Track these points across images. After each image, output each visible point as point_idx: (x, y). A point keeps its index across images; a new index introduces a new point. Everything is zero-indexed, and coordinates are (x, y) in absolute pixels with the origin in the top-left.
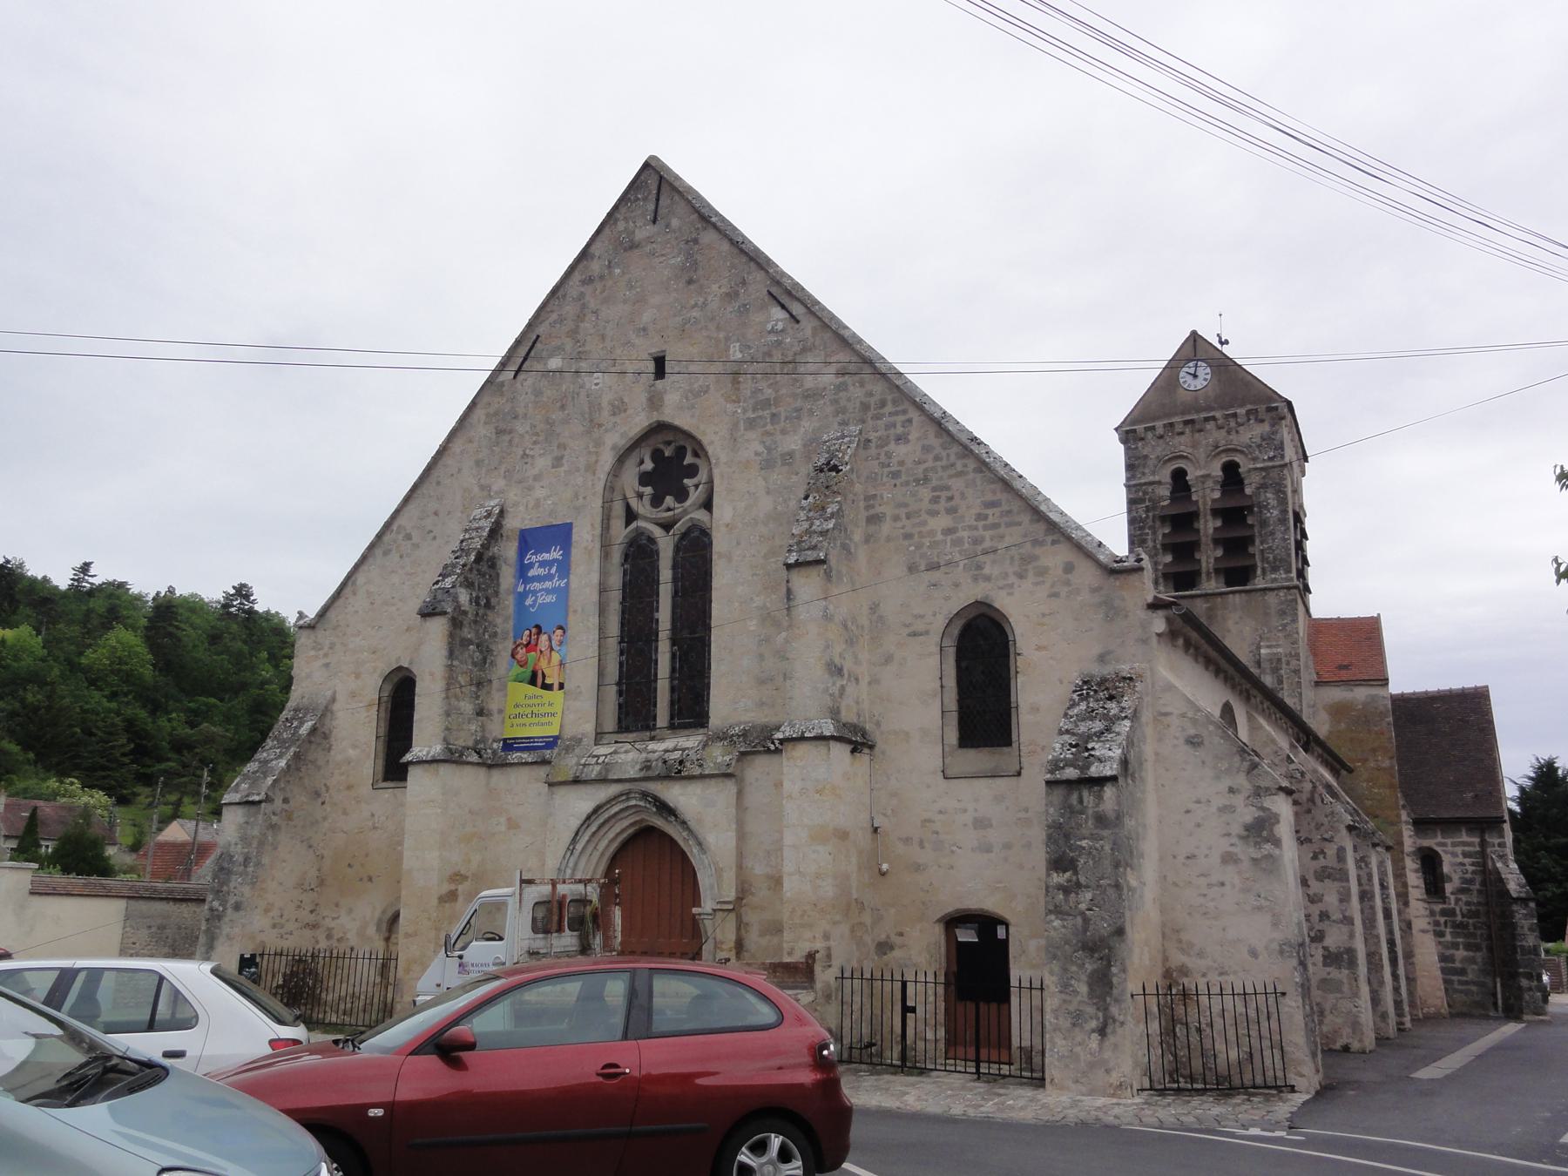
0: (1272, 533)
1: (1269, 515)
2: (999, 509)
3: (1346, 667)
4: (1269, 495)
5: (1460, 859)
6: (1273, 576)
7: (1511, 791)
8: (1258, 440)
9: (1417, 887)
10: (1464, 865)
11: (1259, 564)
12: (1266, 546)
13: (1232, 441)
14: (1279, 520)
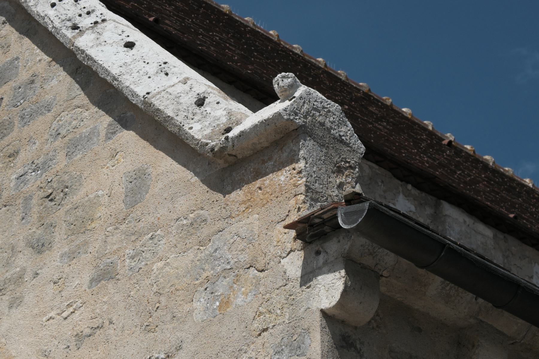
2: (12, 84)
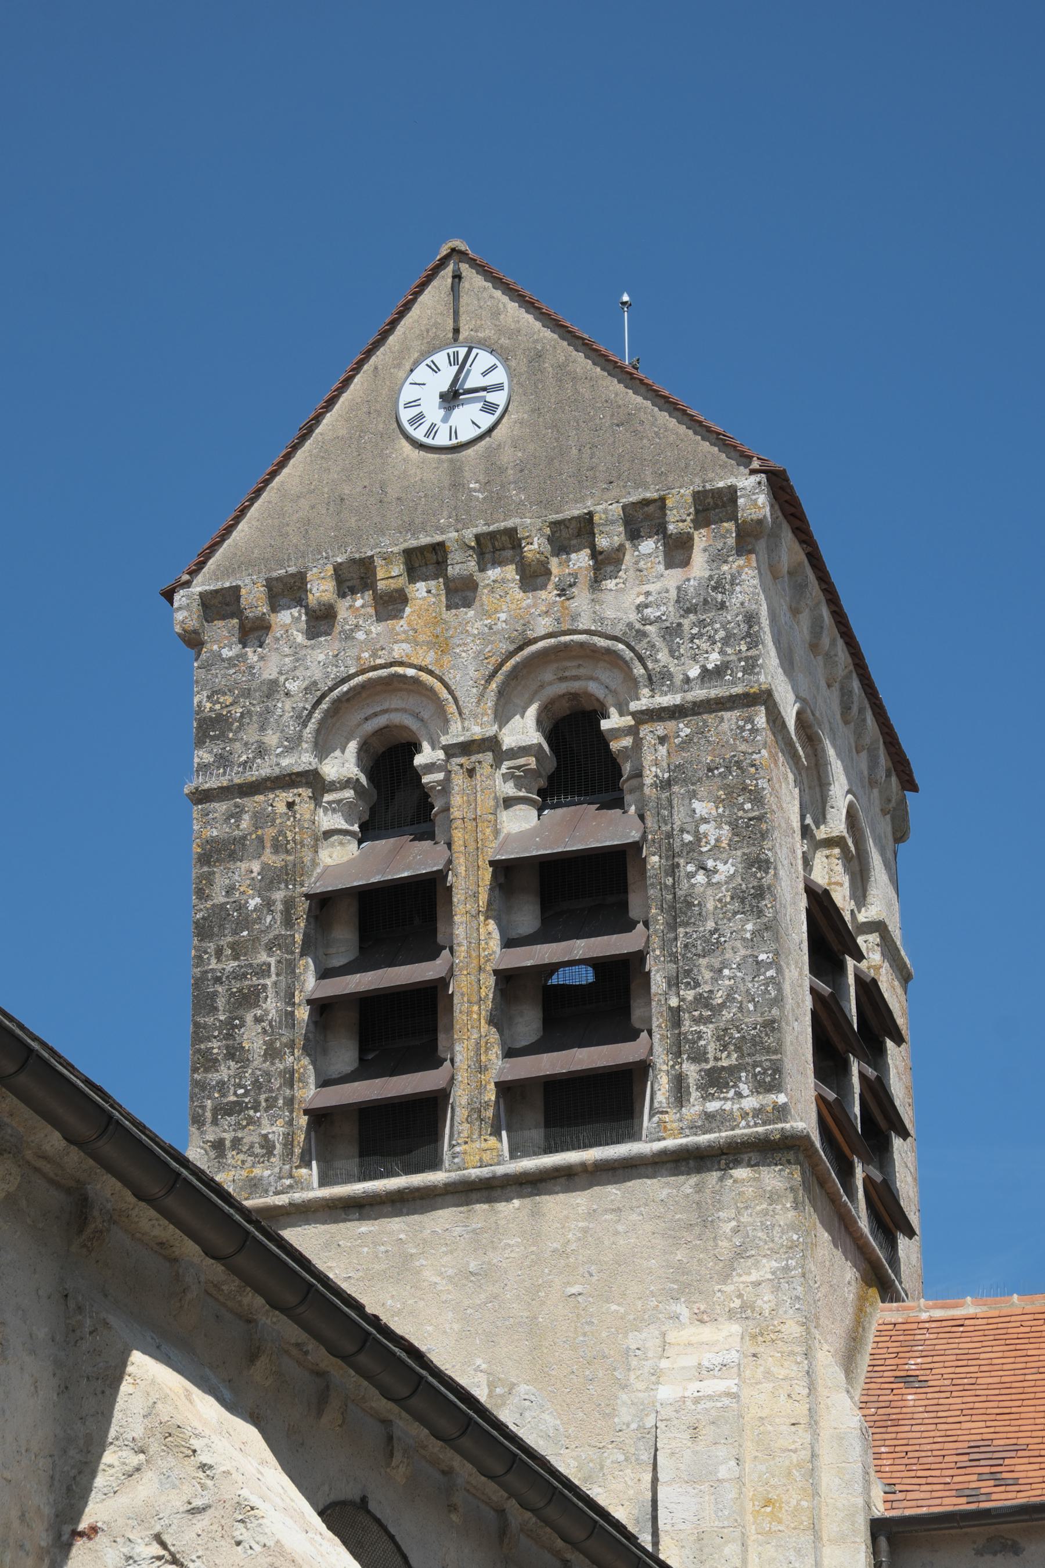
0: (713, 946)
1: (701, 878)
3: (844, 897)
4: (702, 808)
6: (713, 1106)
7: (856, 1160)
8: (669, 612)
11: (662, 1060)
12: (689, 995)
13: (574, 618)
14: (739, 896)
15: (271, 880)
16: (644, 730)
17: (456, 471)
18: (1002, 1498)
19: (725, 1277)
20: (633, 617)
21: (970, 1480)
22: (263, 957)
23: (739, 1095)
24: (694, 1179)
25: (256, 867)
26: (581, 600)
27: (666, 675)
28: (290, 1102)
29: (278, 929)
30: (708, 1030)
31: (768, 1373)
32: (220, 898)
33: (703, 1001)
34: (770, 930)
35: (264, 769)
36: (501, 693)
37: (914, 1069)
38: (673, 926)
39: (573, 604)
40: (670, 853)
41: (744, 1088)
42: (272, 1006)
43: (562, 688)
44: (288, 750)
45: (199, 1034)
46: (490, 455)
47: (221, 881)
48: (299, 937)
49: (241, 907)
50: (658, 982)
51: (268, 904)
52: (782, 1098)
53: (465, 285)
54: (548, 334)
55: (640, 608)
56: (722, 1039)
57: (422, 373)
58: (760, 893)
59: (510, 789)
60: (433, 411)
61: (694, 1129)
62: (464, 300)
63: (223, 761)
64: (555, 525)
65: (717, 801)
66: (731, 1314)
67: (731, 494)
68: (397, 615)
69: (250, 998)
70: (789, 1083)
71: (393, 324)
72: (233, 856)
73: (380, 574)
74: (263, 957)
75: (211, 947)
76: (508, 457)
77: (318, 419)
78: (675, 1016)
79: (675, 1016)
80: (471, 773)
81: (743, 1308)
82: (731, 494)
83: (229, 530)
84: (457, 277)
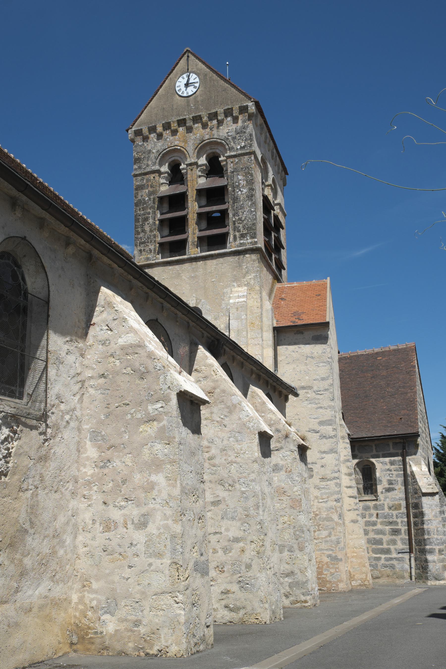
0: (242, 207)
1: (240, 193)
5: (388, 467)
6: (242, 241)
8: (233, 134)
9: (350, 487)
10: (391, 471)
11: (231, 232)
12: (237, 218)
13: (213, 135)
15: (150, 194)
16: (228, 160)
17: (188, 102)
18: (300, 323)
19: (244, 278)
20: (226, 135)
21: (293, 319)
22: (149, 210)
23: (247, 239)
24: (238, 257)
25: (147, 191)
26: (215, 131)
27: (233, 148)
28: (155, 241)
29: (152, 204)
30: (241, 225)
31: (252, 297)
32: (140, 198)
33: (240, 219)
34: (254, 204)
35: (148, 169)
36: (198, 152)
37: (287, 235)
38: (234, 203)
39: (213, 132)
40: (233, 187)
41: (248, 238)
42: (151, 221)
43: (211, 151)
44: (153, 165)
45: (136, 227)
46: (195, 98)
47: (140, 194)
48: (156, 206)
49: (144, 200)
50: (231, 215)
51: (150, 199)
52: (256, 240)
53: (190, 58)
54: (208, 70)
55: (227, 133)
56: (244, 227)
57: (180, 79)
58: (252, 196)
59: (200, 174)
60: (183, 89)
61: (238, 246)
62: (190, 62)
63: (140, 168)
64: (209, 114)
65: (243, 176)
66: (245, 285)
67: (247, 107)
68: (176, 135)
69: (146, 219)
70: (258, 237)
71: (174, 68)
72: (142, 189)
73: (172, 126)
74: (149, 210)
75: (138, 208)
76: (199, 99)
77: (158, 90)
78: (234, 223)
79: (234, 223)
80: (192, 170)
81: (248, 283)
82: (247, 107)
83: (140, 116)
84: (188, 57)
